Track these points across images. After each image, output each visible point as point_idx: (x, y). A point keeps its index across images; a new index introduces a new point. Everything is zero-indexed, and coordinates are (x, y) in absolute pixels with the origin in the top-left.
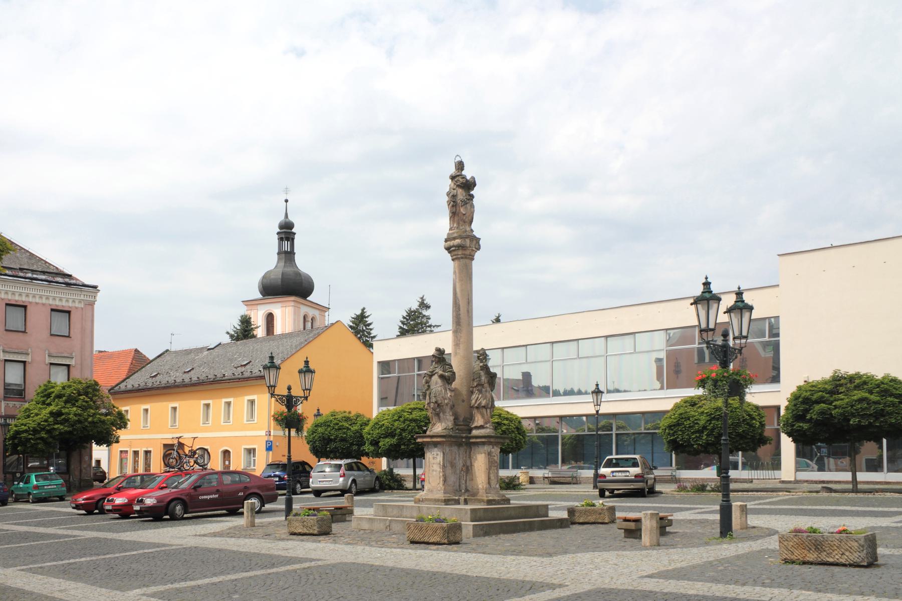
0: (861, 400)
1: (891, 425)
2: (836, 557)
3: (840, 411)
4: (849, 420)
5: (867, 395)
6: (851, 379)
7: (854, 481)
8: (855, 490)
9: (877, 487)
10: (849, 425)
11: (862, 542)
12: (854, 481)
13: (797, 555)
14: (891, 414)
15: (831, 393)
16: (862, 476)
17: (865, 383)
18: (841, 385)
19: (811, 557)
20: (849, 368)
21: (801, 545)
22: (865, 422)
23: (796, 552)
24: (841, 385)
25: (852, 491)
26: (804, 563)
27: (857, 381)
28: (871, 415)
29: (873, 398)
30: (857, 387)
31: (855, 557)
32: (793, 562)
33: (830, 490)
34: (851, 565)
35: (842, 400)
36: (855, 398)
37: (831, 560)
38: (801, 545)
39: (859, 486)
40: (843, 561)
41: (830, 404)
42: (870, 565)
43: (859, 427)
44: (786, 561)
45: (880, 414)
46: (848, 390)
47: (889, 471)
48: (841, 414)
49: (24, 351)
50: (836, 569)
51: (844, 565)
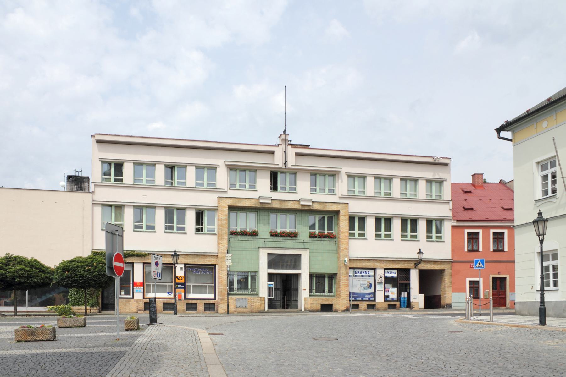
0: (21, 269)
1: (34, 282)
2: (41, 337)
3: (11, 274)
4: (15, 279)
5: (24, 267)
6: (15, 258)
7: (16, 311)
8: (16, 315)
9: (23, 314)
10: (14, 282)
11: (51, 330)
12: (16, 311)
13: (23, 338)
14: (34, 276)
15: (6, 265)
16: (19, 309)
17: (22, 261)
18: (11, 261)
19: (30, 338)
20: (14, 253)
21: (26, 333)
22: (22, 281)
23: (23, 337)
24: (11, 261)
25: (15, 315)
26: (26, 341)
27: (19, 260)
28: (25, 277)
29: (27, 269)
30: (19, 263)
31: (48, 337)
32: (21, 341)
33: (4, 315)
34: (46, 340)
35: (12, 269)
36: (18, 268)
37: (38, 339)
38: (26, 333)
39: (18, 314)
40: (43, 339)
41: (6, 270)
42: (84, 327)
43: (20, 283)
44: (18, 341)
45: (29, 277)
46: (14, 264)
47: (29, 305)
48: (11, 276)
49: (526, 132)
50: (42, 342)
51: (44, 341)
